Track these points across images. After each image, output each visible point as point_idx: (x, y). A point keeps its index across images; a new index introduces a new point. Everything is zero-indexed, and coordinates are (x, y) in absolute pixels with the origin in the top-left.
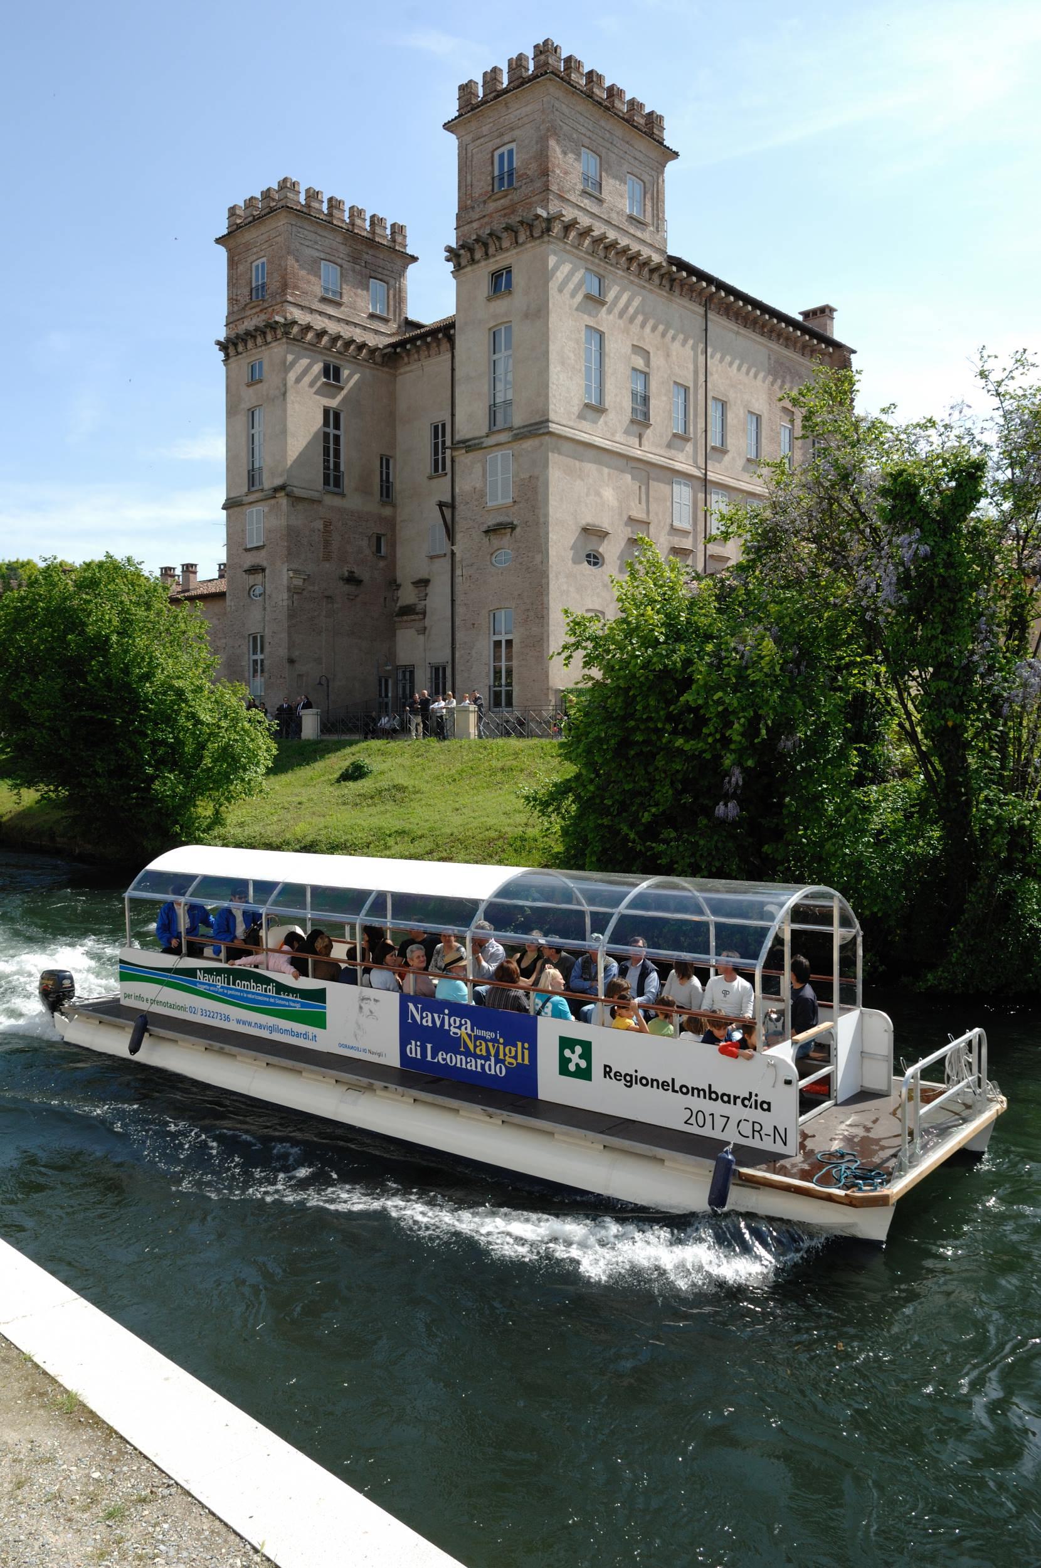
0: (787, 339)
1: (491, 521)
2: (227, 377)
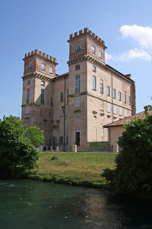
0: (124, 80)
1: (76, 109)
2: (23, 83)
